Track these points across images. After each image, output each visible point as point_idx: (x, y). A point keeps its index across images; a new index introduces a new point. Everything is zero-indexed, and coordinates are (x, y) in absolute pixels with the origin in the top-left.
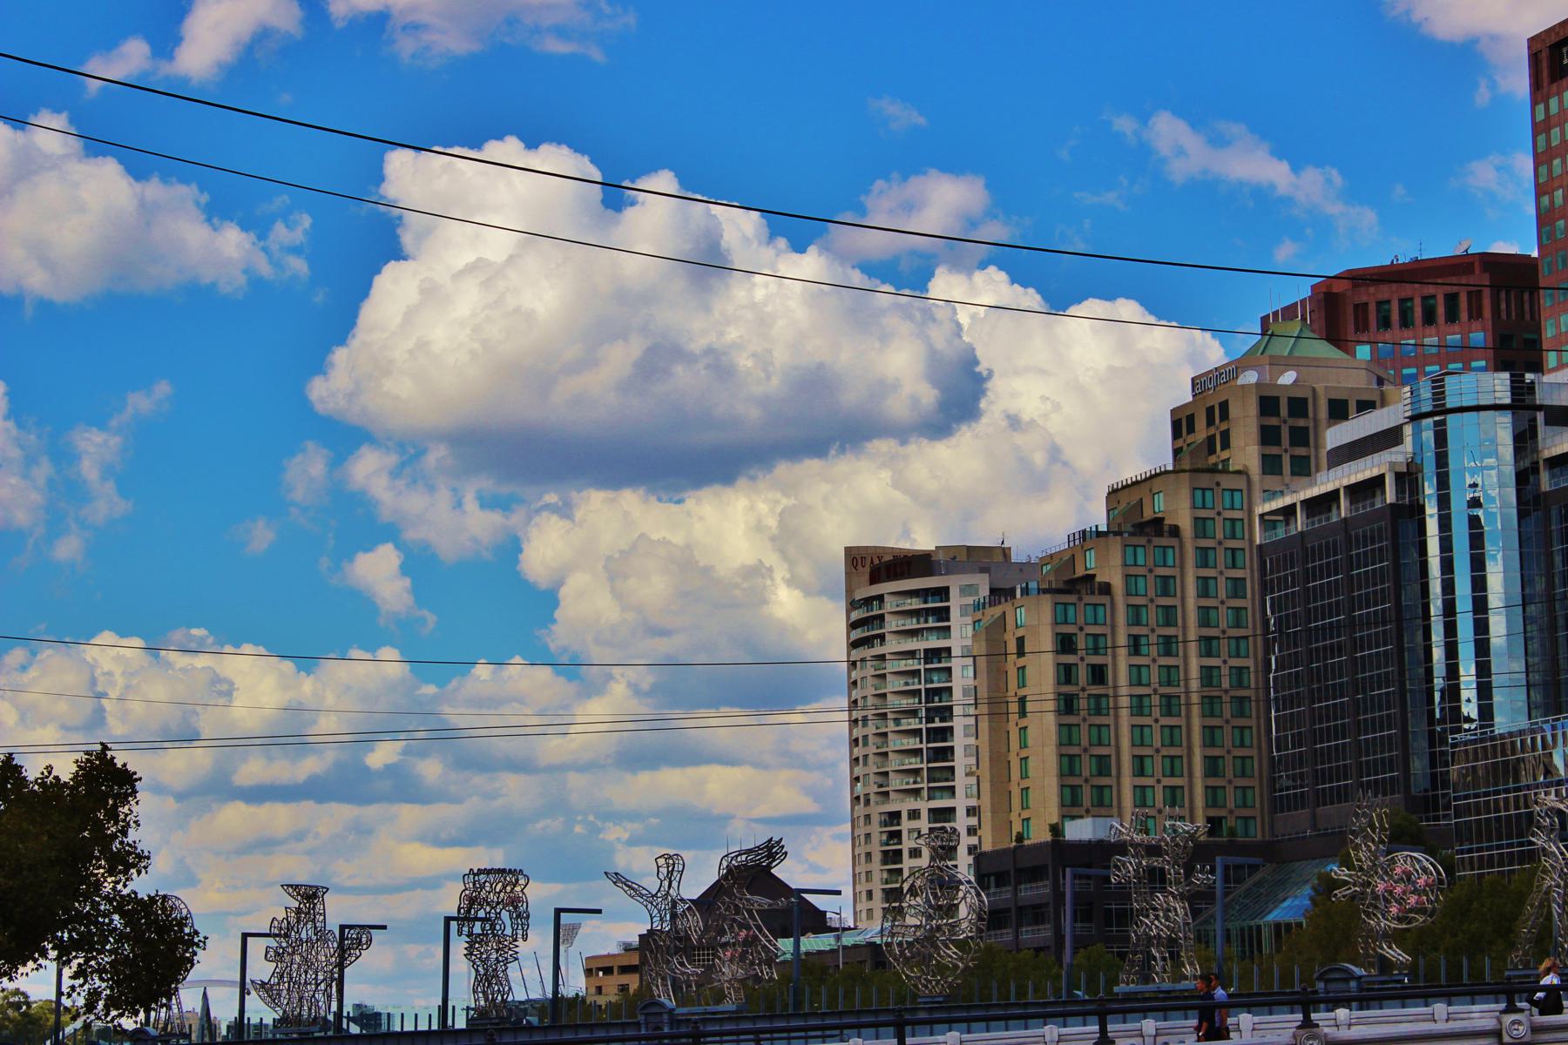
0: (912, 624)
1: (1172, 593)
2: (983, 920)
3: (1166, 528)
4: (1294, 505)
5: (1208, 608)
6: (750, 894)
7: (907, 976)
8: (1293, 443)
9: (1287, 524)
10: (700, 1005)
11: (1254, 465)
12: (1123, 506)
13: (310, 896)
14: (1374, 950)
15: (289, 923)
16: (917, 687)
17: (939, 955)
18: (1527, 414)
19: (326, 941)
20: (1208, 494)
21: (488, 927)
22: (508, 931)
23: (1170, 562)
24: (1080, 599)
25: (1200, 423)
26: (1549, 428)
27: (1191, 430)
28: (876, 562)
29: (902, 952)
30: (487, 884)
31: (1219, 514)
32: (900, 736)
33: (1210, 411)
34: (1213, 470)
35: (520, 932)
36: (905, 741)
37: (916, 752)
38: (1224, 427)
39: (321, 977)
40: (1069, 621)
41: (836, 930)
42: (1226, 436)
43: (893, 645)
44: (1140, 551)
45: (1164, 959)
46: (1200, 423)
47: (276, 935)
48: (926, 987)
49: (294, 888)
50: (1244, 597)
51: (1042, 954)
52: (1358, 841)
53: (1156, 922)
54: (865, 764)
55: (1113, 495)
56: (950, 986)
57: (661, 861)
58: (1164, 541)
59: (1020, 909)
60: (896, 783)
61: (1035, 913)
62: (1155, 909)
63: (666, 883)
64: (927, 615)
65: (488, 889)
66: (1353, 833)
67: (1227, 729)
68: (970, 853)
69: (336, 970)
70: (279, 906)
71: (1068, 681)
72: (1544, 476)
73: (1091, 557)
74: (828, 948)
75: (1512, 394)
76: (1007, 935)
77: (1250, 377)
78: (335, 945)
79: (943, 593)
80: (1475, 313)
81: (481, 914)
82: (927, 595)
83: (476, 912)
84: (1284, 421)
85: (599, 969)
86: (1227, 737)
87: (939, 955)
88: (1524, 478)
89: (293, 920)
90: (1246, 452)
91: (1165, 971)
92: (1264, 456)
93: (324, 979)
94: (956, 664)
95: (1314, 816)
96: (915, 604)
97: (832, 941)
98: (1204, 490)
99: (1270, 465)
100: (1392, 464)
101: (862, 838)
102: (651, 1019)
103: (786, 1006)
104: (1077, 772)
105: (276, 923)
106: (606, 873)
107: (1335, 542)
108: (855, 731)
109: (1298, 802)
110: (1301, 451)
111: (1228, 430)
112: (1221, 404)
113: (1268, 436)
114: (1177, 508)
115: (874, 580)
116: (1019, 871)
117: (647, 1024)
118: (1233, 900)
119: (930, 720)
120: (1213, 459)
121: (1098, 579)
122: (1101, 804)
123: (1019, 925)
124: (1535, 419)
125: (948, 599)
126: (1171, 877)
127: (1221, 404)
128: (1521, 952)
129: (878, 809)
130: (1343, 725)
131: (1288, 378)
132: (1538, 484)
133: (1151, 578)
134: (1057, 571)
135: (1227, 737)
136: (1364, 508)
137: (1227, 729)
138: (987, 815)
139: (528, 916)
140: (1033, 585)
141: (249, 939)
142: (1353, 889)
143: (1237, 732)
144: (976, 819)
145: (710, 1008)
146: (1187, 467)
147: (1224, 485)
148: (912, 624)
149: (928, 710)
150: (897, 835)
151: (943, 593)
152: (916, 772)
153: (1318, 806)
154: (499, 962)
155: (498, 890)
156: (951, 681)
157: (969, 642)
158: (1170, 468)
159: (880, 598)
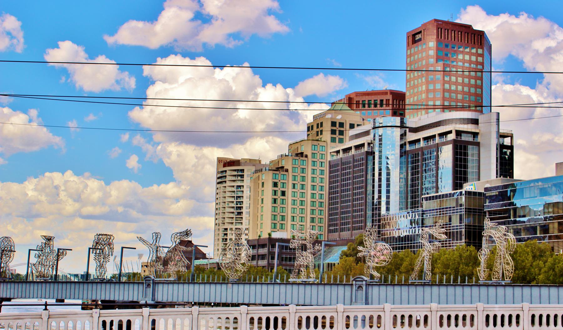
0: (234, 178)
2: (250, 257)
3: (304, 155)
5: (314, 177)
6: (180, 245)
7: (226, 273)
8: (339, 134)
9: (337, 155)
10: (163, 278)
12: (293, 149)
13: (49, 239)
14: (369, 272)
15: (42, 247)
16: (234, 195)
17: (236, 267)
18: (404, 129)
19: (53, 253)
20: (316, 146)
21: (101, 251)
22: (107, 253)
23: (305, 164)
24: (280, 173)
25: (315, 127)
26: (410, 133)
27: (312, 129)
28: (225, 161)
29: (225, 266)
30: (102, 239)
31: (318, 152)
32: (231, 176)
33: (318, 124)
34: (317, 140)
35: (110, 253)
36: (230, 215)
37: (233, 213)
38: (321, 129)
39: (51, 264)
40: (276, 178)
41: (208, 259)
42: (321, 131)
43: (228, 184)
44: (297, 161)
45: (304, 271)
46: (315, 127)
47: (39, 250)
48: (232, 276)
50: (324, 175)
51: (264, 268)
52: (367, 239)
53: (303, 260)
54: (219, 215)
55: (290, 146)
56: (239, 276)
57: (154, 234)
58: (304, 158)
59: (259, 256)
60: (227, 220)
61: (263, 257)
62: (302, 256)
63: (155, 241)
64: (238, 176)
65: (102, 240)
66: (365, 236)
67: (317, 210)
68: (245, 240)
69: (56, 261)
70: (41, 241)
71: (275, 195)
72: (408, 146)
73: (284, 161)
74: (206, 263)
75: (401, 123)
76: (254, 263)
77: (329, 116)
78: (56, 254)
79: (242, 171)
80: (388, 105)
81: (99, 247)
82: (238, 171)
83: (98, 247)
84: (337, 128)
85: (145, 266)
86: (317, 212)
87: (236, 267)
89: (44, 246)
90: (327, 136)
91: (304, 275)
93: (52, 264)
94: (245, 189)
95: (340, 235)
96: (235, 173)
97: (207, 261)
98: (315, 145)
99: (333, 140)
100: (367, 140)
101: (217, 235)
102: (147, 282)
103: (189, 279)
104: (276, 219)
105: (38, 247)
106: (137, 237)
107: (350, 161)
108: (216, 217)
109: (335, 231)
110: (341, 137)
112: (321, 123)
113: (333, 132)
114: (307, 149)
115: (224, 166)
116: (259, 245)
117: (146, 283)
118: (317, 256)
119: (237, 204)
120: (317, 138)
121: (285, 168)
122: (282, 228)
123: (258, 260)
124: (406, 131)
125: (244, 172)
126: (308, 247)
127: (321, 123)
128: (414, 275)
129: (222, 227)
130: (349, 210)
131: (339, 117)
132: (405, 148)
133: (299, 168)
134: (274, 165)
135: (317, 212)
136: (359, 152)
137: (317, 210)
138: (251, 230)
139: (113, 249)
140: (267, 168)
141: (31, 251)
142: (364, 253)
143: (320, 211)
144: (248, 231)
145: (166, 279)
146: (311, 139)
147: (320, 145)
148: (234, 178)
149: (236, 202)
150: (226, 234)
151: (242, 171)
152: (232, 218)
153: (353, 230)
154: (103, 262)
155: (105, 240)
157: (249, 184)
158: (306, 139)
159: (226, 171)
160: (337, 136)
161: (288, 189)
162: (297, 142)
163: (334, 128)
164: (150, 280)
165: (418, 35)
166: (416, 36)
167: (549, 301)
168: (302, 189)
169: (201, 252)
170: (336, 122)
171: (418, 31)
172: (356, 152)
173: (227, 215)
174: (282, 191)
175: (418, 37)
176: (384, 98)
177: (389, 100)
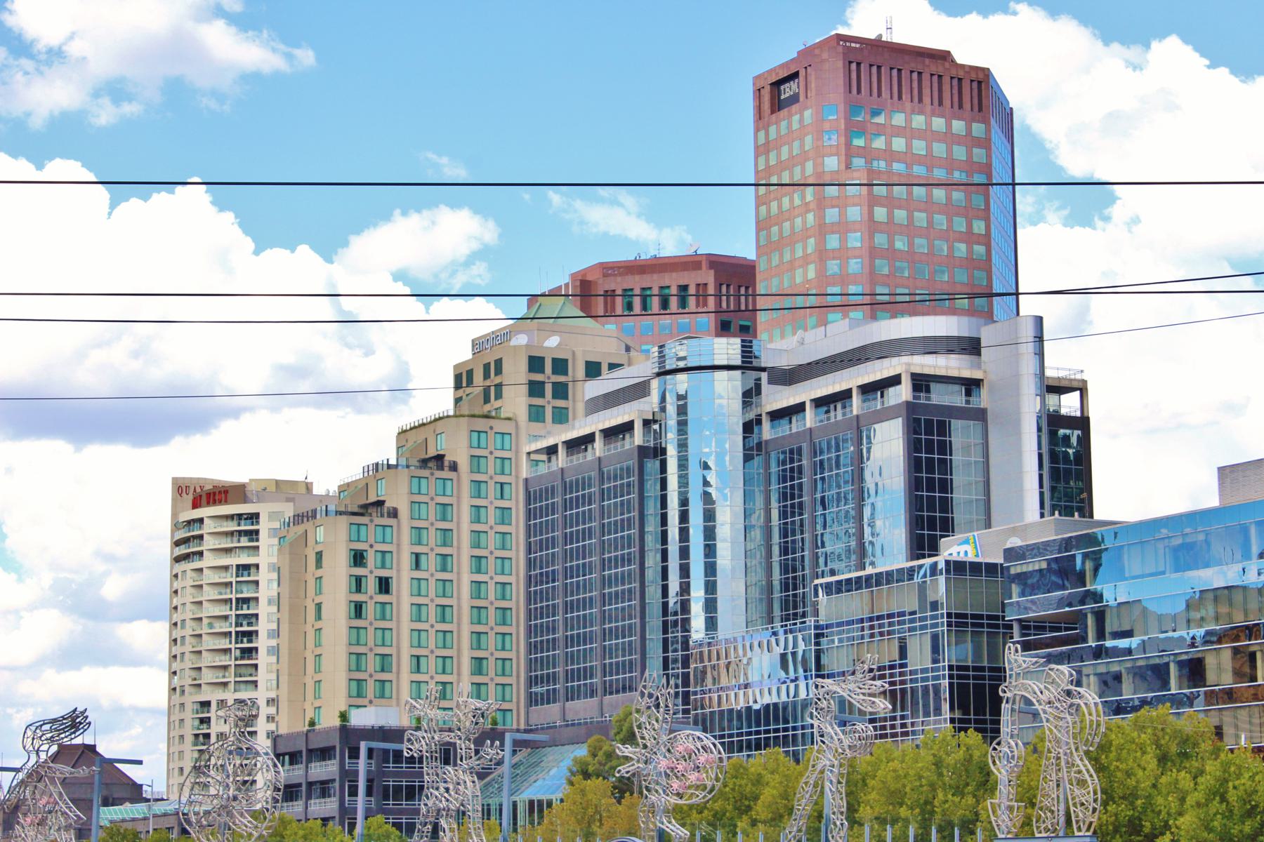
8: (555, 396)
27: (470, 382)
33: (487, 367)
43: (209, 560)
58: (446, 474)
84: (548, 376)
90: (516, 401)
99: (536, 414)
100: (641, 412)
110: (560, 403)
113: (535, 389)
114: (457, 447)
124: (759, 379)
147: (496, 430)
150: (205, 721)
159: (201, 521)
160: (548, 402)
162: (424, 424)
163: (538, 377)
165: (787, 85)
166: (782, 87)
169: (125, 781)
170: (542, 359)
173: (207, 660)
174: (380, 579)
175: (788, 90)
176: (691, 279)
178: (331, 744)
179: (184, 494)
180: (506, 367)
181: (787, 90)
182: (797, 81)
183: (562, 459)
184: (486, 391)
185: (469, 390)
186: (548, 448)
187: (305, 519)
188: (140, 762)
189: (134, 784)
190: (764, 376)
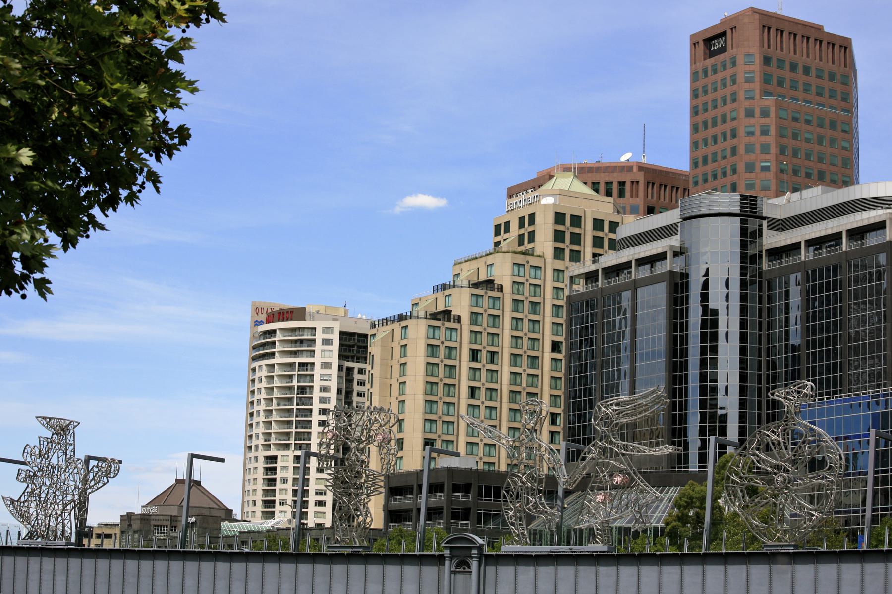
1: (538, 313)
4: (597, 271)
8: (572, 242)
11: (549, 253)
25: (514, 226)
27: (507, 229)
28: (270, 311)
31: (527, 280)
33: (522, 219)
38: (531, 229)
43: (278, 360)
46: (514, 226)
49: (47, 421)
58: (495, 294)
84: (567, 228)
88: (749, 260)
92: (555, 249)
99: (558, 253)
100: (672, 247)
102: (456, 553)
110: (576, 248)
111: (534, 231)
113: (559, 236)
124: (761, 225)
147: (531, 263)
156: (313, 382)
161: (460, 361)
162: (476, 258)
163: (560, 245)
164: (470, 549)
165: (717, 40)
166: (712, 42)
167: (318, 512)
168: (492, 361)
169: (223, 507)
171: (719, 32)
172: (609, 283)
174: (477, 361)
175: (717, 45)
176: (628, 178)
177: (638, 182)
178: (409, 483)
179: (260, 313)
180: (538, 219)
181: (716, 44)
182: (724, 38)
183: (601, 282)
184: (521, 237)
185: (506, 236)
186: (586, 274)
187: (392, 319)
188: (222, 460)
189: (227, 509)
190: (765, 223)
